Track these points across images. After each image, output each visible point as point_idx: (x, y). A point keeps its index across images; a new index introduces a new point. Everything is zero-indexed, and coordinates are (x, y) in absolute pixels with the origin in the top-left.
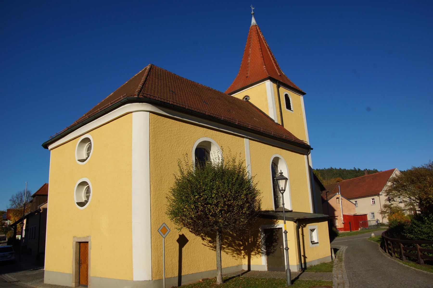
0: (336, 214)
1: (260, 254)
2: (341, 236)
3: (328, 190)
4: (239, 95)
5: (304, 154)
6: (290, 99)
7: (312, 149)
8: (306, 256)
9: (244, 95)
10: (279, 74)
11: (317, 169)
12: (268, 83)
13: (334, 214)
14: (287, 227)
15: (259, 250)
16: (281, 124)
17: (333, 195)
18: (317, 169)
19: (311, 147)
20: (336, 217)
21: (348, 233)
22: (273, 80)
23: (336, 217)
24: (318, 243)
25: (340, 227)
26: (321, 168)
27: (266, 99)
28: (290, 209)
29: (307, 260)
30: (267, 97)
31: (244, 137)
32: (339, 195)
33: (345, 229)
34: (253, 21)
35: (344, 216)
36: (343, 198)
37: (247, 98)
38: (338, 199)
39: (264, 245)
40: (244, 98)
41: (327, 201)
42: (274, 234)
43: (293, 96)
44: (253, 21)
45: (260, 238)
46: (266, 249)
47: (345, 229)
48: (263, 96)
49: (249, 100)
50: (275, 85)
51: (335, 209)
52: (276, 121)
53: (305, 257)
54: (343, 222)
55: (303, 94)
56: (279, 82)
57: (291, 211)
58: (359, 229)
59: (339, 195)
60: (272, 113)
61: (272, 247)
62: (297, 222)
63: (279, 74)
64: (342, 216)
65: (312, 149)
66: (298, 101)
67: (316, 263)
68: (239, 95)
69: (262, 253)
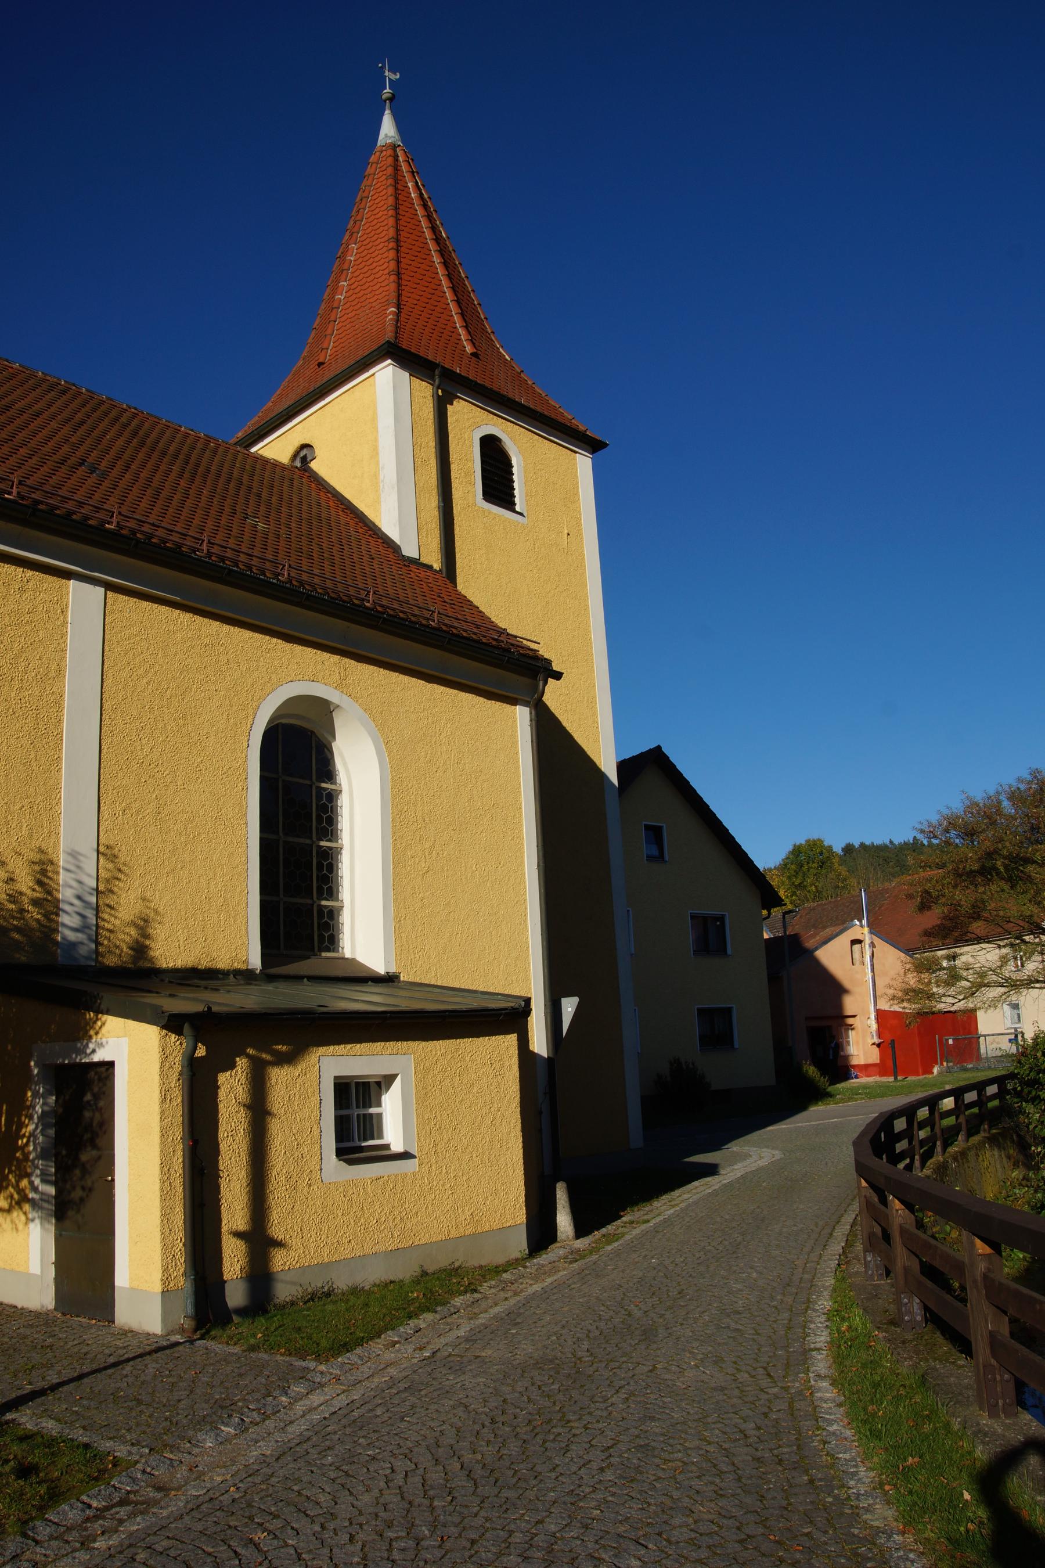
0: (850, 1004)
1: (27, 1207)
2: (842, 1101)
3: (790, 907)
4: (277, 448)
5: (513, 702)
6: (514, 462)
7: (558, 676)
8: (277, 1229)
9: (296, 444)
10: (469, 349)
11: (862, 845)
12: (386, 376)
13: (839, 1006)
14: (133, 1053)
15: (24, 1183)
16: (437, 566)
17: (838, 929)
18: (862, 845)
19: (556, 667)
20: (850, 1021)
21: (879, 1085)
22: (413, 362)
23: (850, 1021)
24: (405, 1156)
25: (862, 1062)
26: (878, 841)
27: (375, 452)
28: (379, 966)
29: (280, 1261)
30: (376, 440)
31: (67, 575)
32: (860, 929)
33: (881, 1068)
34: (388, 130)
35: (880, 1015)
36: (877, 941)
37: (304, 453)
38: (856, 947)
39: (44, 1155)
40: (294, 457)
41: (808, 955)
42: (88, 1097)
43: (522, 445)
44: (388, 130)
45: (31, 1118)
46: (55, 1184)
47: (881, 1068)
48: (367, 442)
49: (313, 465)
50: (425, 391)
51: (846, 983)
52: (410, 550)
53: (260, 1241)
54: (876, 1040)
55: (594, 446)
56: (448, 381)
57: (390, 979)
58: (935, 1070)
59: (860, 929)
60: (396, 513)
61: (78, 1172)
62: (187, 1028)
63: (469, 349)
64: (873, 1016)
65: (558, 676)
66: (558, 478)
67: (371, 1276)
68: (277, 448)
69: (33, 1203)
